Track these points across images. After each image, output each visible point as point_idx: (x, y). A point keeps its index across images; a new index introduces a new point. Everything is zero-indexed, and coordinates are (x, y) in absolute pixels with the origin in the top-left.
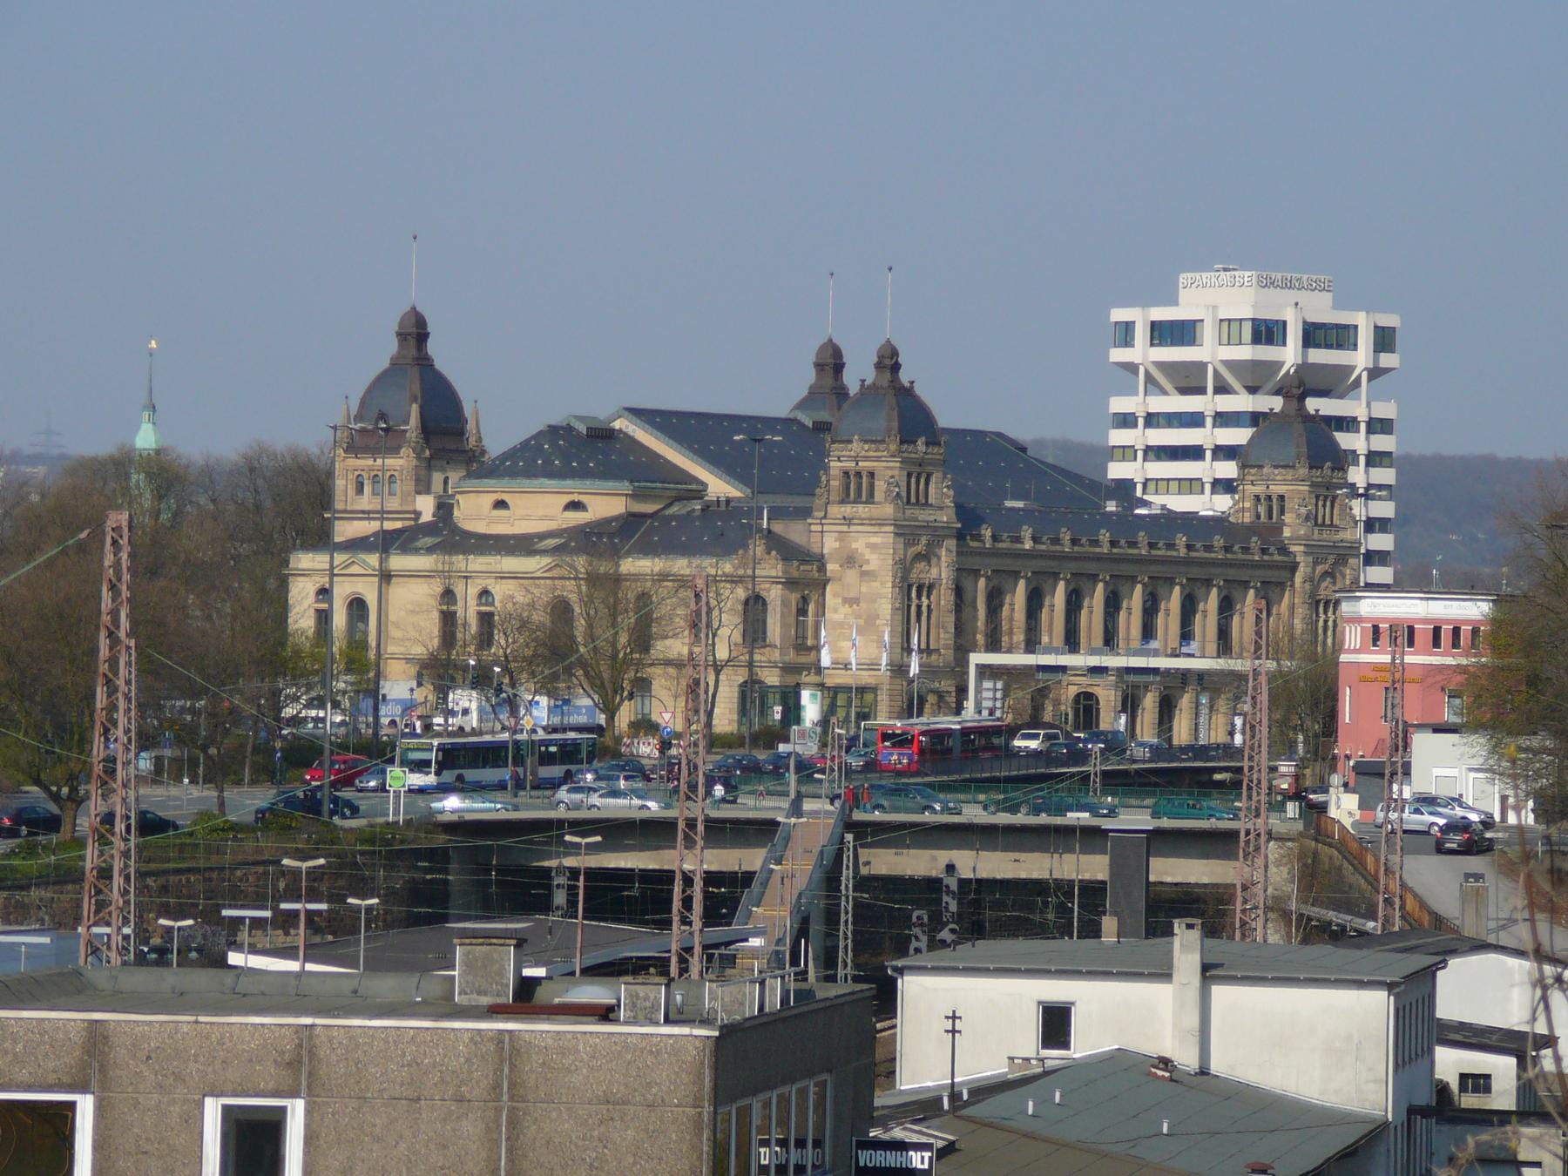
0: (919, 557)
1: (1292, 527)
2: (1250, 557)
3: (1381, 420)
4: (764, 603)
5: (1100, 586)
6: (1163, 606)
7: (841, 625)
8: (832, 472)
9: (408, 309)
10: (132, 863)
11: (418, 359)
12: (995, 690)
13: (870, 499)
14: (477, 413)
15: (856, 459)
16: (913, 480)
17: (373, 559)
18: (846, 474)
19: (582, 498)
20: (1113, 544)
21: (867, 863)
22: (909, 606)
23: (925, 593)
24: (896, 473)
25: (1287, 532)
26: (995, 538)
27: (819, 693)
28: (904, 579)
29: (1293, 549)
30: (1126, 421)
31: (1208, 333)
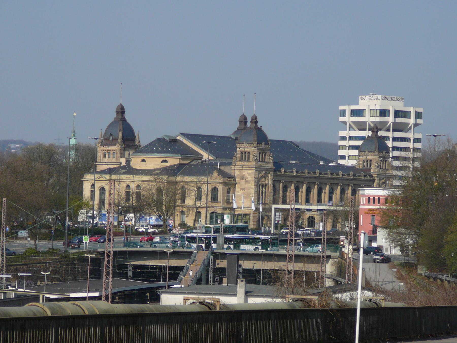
0: (262, 177)
1: (373, 169)
2: (361, 178)
3: (417, 139)
4: (217, 190)
5: (316, 186)
6: (335, 192)
7: (240, 196)
8: (238, 152)
9: (119, 104)
10: (4, 262)
11: (121, 119)
12: (279, 215)
13: (248, 160)
14: (139, 134)
15: (245, 148)
16: (261, 155)
17: (107, 176)
18: (242, 153)
19: (166, 159)
20: (320, 173)
21: (218, 264)
22: (259, 191)
23: (264, 187)
24: (256, 152)
25: (372, 171)
26: (285, 172)
27: (229, 216)
28: (258, 183)
29: (374, 176)
30: (343, 138)
31: (367, 113)
